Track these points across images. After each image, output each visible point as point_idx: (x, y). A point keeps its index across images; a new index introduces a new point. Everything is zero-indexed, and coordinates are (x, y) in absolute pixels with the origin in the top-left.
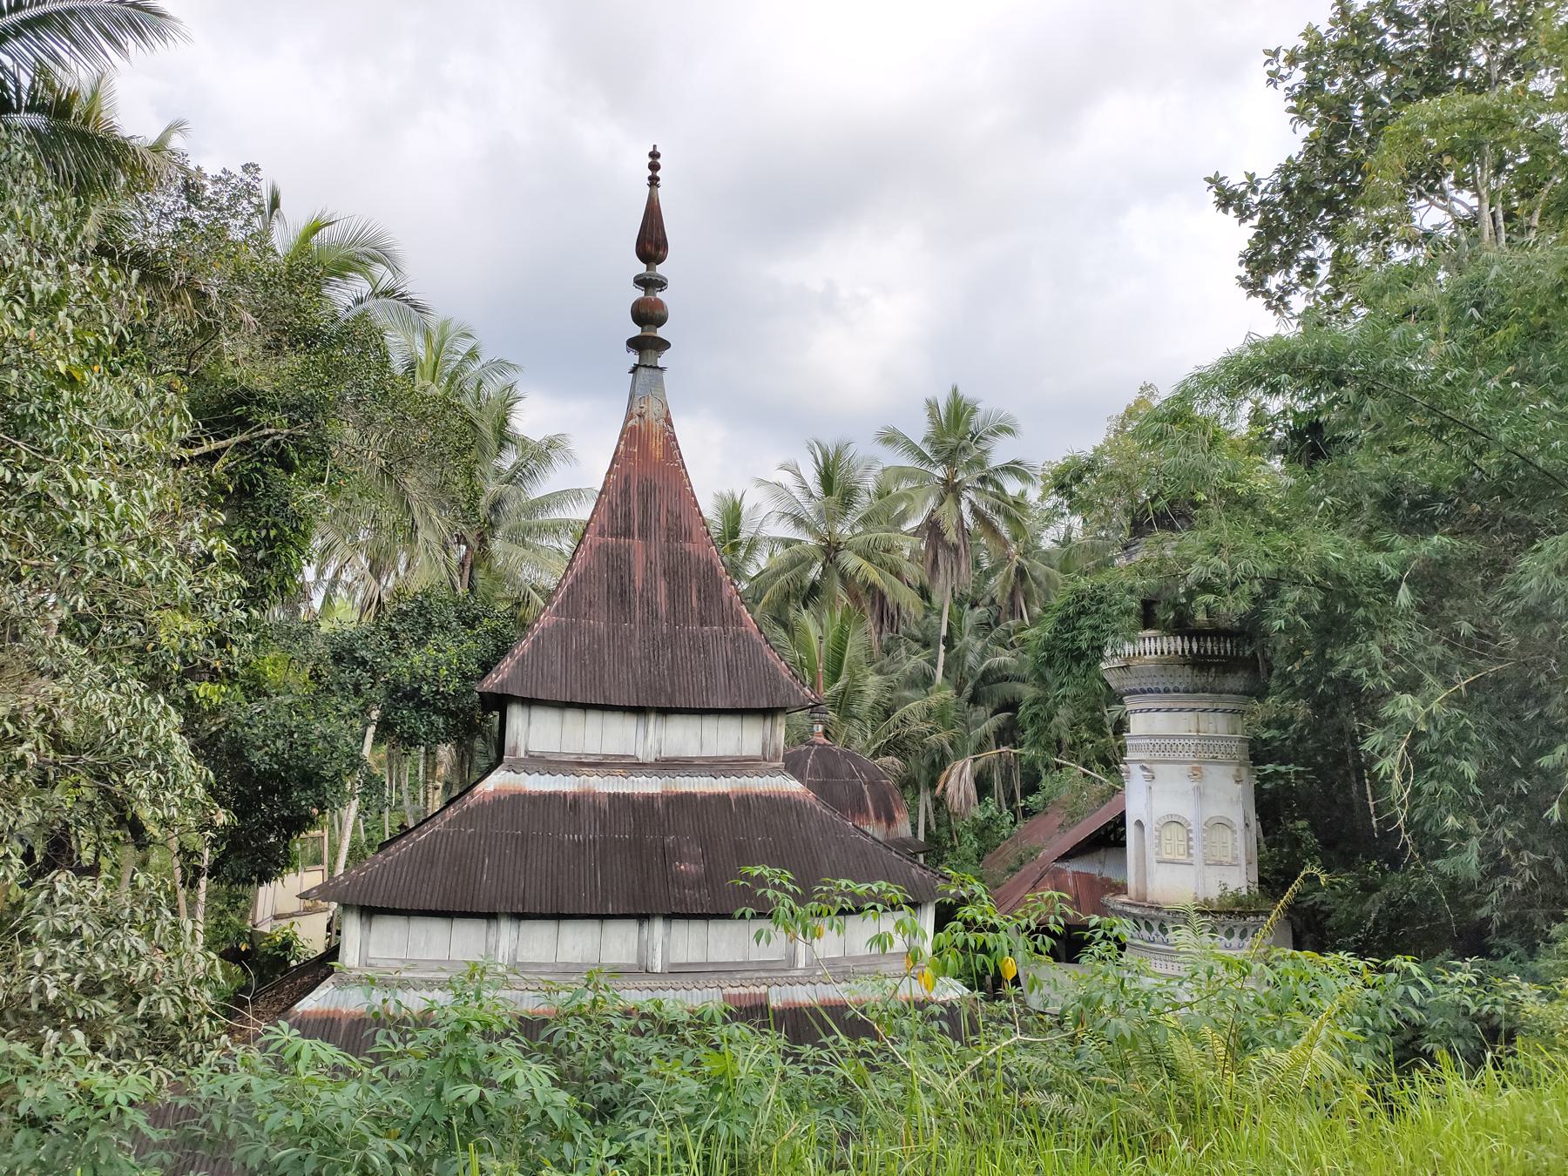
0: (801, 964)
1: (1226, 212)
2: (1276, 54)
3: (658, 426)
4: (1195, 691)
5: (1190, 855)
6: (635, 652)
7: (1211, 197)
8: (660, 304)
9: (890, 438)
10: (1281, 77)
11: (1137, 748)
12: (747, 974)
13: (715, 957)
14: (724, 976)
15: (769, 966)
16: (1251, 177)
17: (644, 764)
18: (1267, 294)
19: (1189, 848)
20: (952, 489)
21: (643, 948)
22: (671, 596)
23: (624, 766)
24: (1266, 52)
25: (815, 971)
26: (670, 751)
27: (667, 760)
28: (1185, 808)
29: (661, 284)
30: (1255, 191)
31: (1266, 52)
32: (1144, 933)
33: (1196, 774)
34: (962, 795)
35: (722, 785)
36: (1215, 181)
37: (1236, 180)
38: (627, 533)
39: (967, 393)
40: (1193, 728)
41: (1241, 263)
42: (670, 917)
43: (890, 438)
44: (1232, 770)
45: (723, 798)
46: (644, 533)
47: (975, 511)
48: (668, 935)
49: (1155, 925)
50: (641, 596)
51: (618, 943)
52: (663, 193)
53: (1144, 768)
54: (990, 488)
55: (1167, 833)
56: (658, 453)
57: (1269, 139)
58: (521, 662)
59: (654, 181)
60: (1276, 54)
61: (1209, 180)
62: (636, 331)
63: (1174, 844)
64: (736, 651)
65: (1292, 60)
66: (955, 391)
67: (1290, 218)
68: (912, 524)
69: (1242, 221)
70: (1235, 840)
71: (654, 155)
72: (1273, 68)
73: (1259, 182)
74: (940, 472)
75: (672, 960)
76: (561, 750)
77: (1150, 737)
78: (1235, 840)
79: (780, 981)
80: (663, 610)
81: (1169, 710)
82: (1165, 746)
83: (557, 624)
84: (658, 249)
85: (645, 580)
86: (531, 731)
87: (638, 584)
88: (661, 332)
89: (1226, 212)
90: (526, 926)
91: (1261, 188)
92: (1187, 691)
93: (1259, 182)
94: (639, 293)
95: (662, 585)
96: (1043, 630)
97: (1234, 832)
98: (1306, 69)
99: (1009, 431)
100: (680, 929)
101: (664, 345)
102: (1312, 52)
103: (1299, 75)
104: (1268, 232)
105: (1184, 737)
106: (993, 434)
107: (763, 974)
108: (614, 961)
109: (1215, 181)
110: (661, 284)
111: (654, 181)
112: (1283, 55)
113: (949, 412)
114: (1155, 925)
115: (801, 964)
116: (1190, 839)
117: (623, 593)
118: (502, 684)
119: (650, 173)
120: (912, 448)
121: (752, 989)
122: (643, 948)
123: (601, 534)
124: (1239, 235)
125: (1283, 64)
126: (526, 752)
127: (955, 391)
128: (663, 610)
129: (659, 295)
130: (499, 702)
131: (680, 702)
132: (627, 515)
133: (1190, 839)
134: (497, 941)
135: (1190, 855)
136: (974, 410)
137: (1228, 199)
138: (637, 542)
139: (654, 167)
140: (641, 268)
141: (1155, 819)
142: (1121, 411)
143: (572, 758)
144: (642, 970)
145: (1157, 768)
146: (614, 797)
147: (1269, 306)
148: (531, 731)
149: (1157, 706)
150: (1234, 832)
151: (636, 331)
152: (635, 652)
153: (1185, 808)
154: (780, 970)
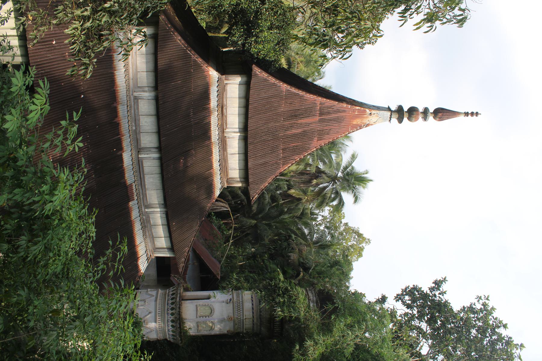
0: (146, 210)
1: (433, 283)
2: (487, 299)
3: (366, 121)
4: (260, 318)
5: (200, 317)
6: (272, 124)
7: (439, 278)
8: (417, 119)
9: (354, 157)
10: (478, 301)
11: (238, 296)
12: (141, 191)
13: (147, 177)
14: (139, 182)
15: (145, 199)
16: (445, 293)
17: (223, 132)
18: (402, 294)
19: (203, 317)
20: (334, 179)
21: (147, 150)
22: (295, 135)
23: (222, 125)
24: (488, 296)
25: (145, 216)
26: (229, 142)
27: (226, 141)
28: (217, 315)
29: (425, 118)
30: (440, 294)
31: (488, 296)
32: (170, 302)
33: (230, 319)
34: (215, 207)
35: (216, 165)
36: (445, 280)
37: (444, 287)
38: (321, 114)
39: (370, 184)
40: (246, 317)
41: (414, 286)
42: (161, 159)
43: (354, 157)
44: (232, 329)
45: (211, 167)
46: (321, 121)
47: (325, 188)
48: (154, 159)
49: (173, 301)
50: (295, 123)
51: (149, 140)
52: (462, 117)
53: (231, 300)
54: (333, 196)
55: (207, 308)
56: (355, 122)
57: (457, 299)
58: (266, 80)
59: (467, 114)
60: (487, 299)
61: (445, 278)
62: (406, 109)
63: (203, 311)
64: (273, 165)
65: (484, 305)
66: (371, 180)
67: (427, 304)
68: (321, 166)
69: (430, 289)
70: (207, 331)
71: (477, 114)
72: (483, 298)
73: (443, 295)
74: (340, 174)
75: (144, 162)
76: (227, 94)
77: (242, 301)
78: (207, 331)
79: (139, 203)
80: (288, 132)
81: (253, 309)
82: (238, 306)
83: (282, 92)
84: (440, 118)
85: (301, 124)
86: (234, 85)
87: (300, 121)
88: (405, 119)
89: (433, 283)
90: (153, 102)
91: (441, 296)
92: (260, 315)
93: (443, 295)
94: (421, 110)
95: (299, 131)
96: (283, 282)
97: (210, 331)
98: (481, 308)
99: (356, 201)
100: (156, 163)
101: (400, 120)
102: (487, 311)
103: (479, 306)
104: (425, 296)
105: (243, 314)
106: (355, 195)
107: (141, 197)
108: (142, 138)
109: (445, 280)
110: (425, 118)
111: (467, 114)
112: (487, 302)
113: (363, 178)
114: (173, 301)
115: (146, 210)
116: (206, 317)
117: (296, 116)
118: (256, 75)
119: (470, 112)
120: (350, 164)
121: (135, 194)
122: (147, 150)
123: (321, 104)
124: (425, 286)
125: (483, 301)
126: (227, 84)
127: (371, 180)
128: (288, 132)
129: (420, 118)
130: (247, 73)
131: (250, 147)
132: (329, 113)
133: (206, 317)
134: (146, 91)
135: (200, 317)
136: (364, 187)
137: (438, 284)
138: (317, 118)
139: (472, 114)
140: (431, 110)
141: (212, 304)
142: (360, 232)
143: (225, 103)
144: (139, 150)
145: (231, 305)
146: (209, 124)
147: (398, 295)
148: (234, 85)
149: (254, 304)
150: (210, 331)
151: (406, 109)
152: (272, 124)
153: (217, 315)
154: (144, 204)
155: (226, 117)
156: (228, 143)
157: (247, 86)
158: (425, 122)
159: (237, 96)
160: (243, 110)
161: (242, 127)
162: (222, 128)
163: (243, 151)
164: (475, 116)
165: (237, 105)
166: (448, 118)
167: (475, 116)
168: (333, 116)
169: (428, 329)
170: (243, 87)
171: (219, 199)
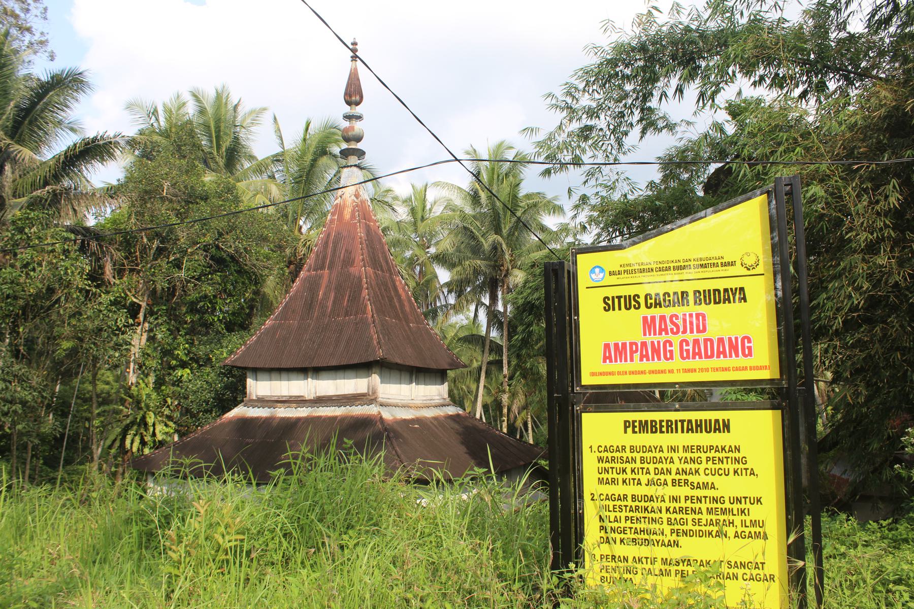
86: (258, 387)
132: (325, 257)
148: (258, 387)
155: (291, 397)
156: (323, 394)
157: (257, 371)
158: (364, 117)
159: (269, 382)
160: (284, 375)
161: (302, 376)
162: (300, 401)
163: (332, 374)
164: (357, 47)
165: (278, 383)
166: (769, 344)
167: (357, 47)
168: (329, 251)
169: (613, 212)
170: (260, 375)
171: (488, 343)
